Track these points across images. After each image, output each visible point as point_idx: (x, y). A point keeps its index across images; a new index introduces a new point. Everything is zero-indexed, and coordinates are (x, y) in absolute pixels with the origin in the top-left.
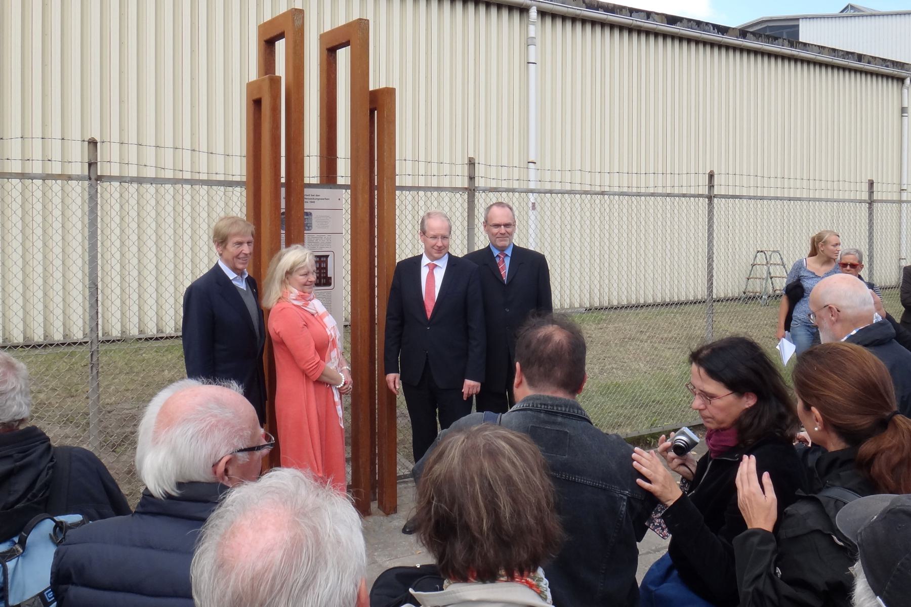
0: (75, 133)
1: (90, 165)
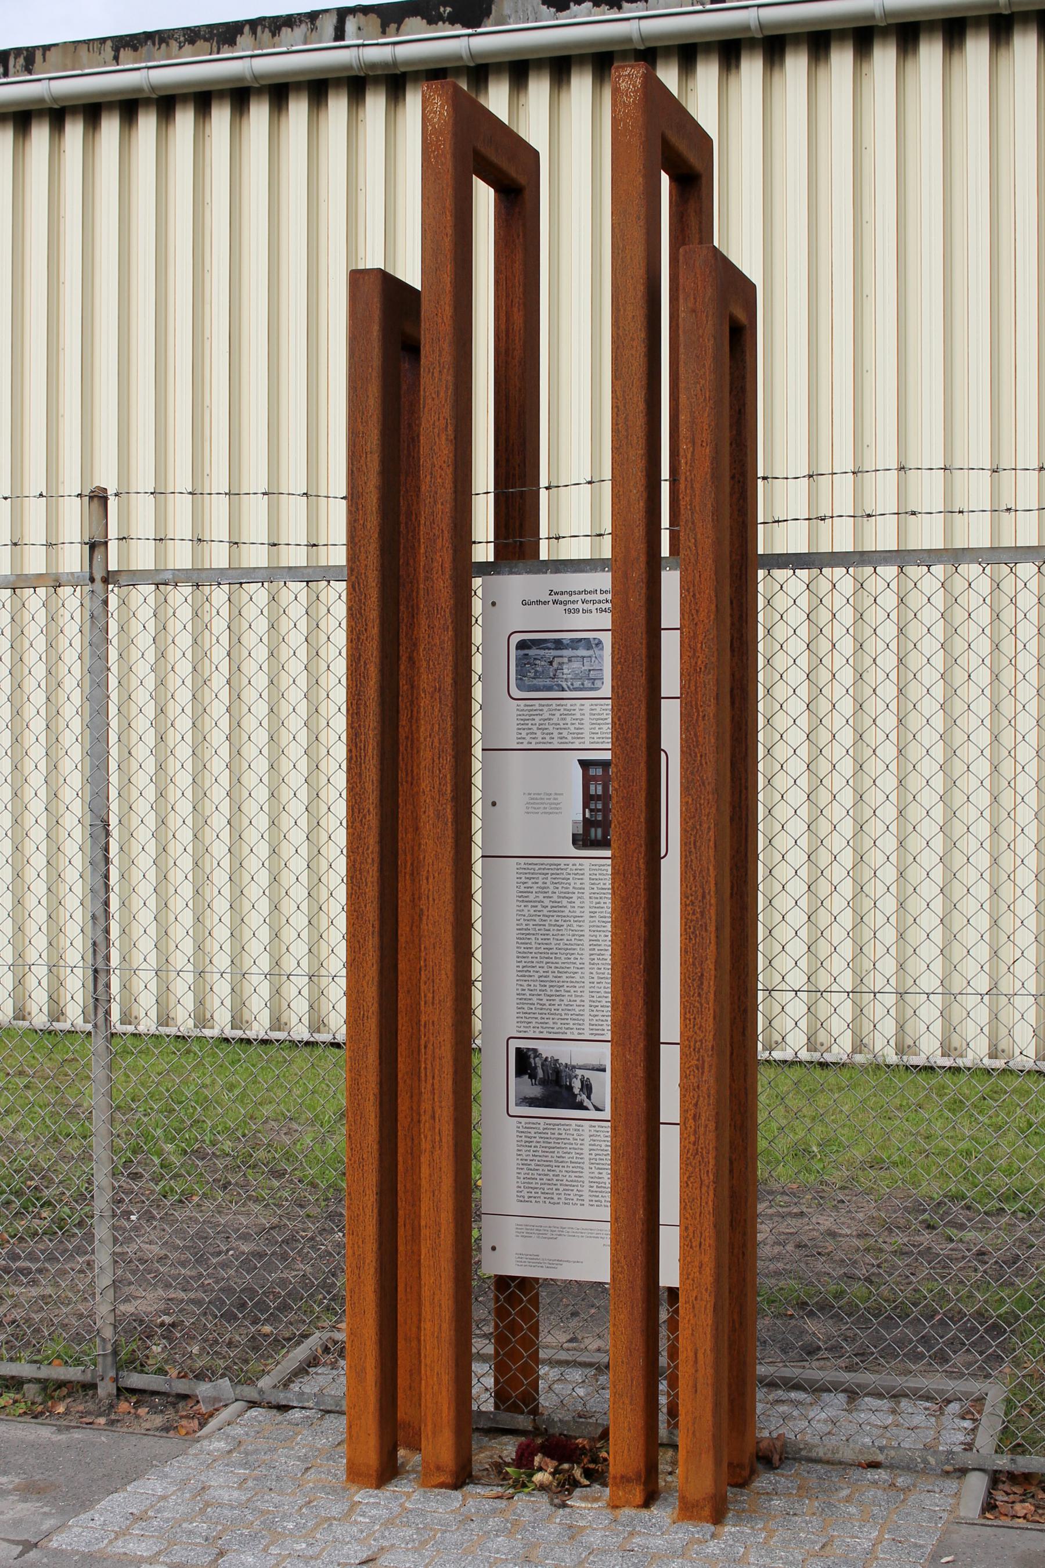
0: (72, 483)
1: (93, 546)
